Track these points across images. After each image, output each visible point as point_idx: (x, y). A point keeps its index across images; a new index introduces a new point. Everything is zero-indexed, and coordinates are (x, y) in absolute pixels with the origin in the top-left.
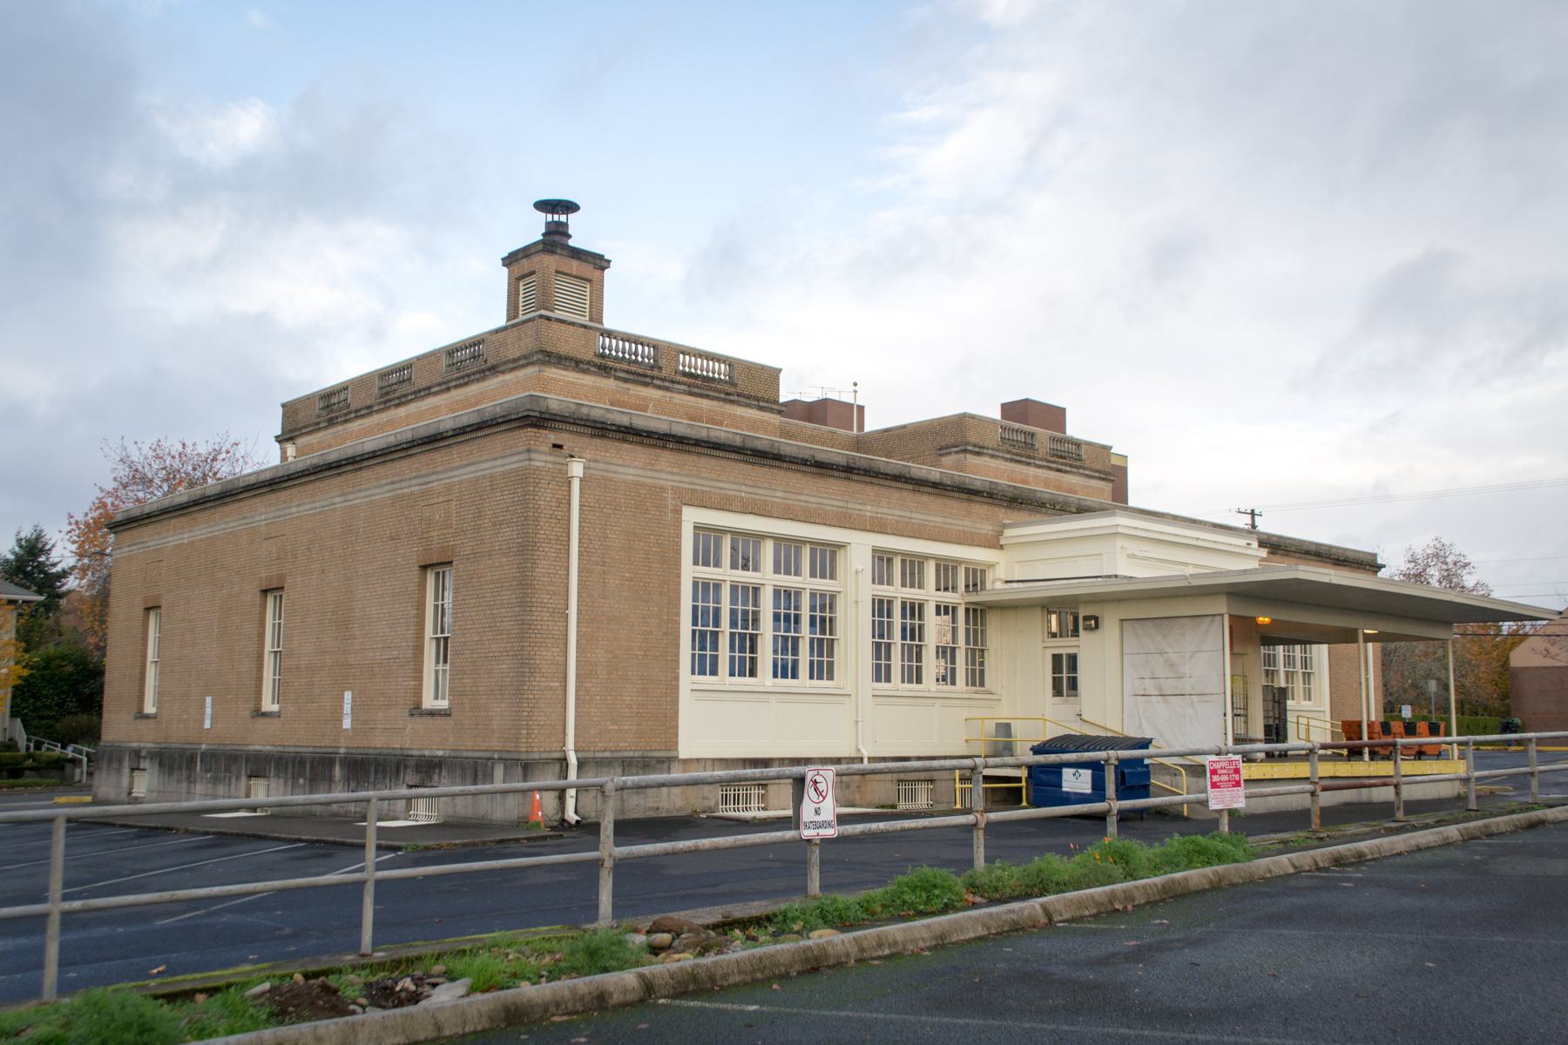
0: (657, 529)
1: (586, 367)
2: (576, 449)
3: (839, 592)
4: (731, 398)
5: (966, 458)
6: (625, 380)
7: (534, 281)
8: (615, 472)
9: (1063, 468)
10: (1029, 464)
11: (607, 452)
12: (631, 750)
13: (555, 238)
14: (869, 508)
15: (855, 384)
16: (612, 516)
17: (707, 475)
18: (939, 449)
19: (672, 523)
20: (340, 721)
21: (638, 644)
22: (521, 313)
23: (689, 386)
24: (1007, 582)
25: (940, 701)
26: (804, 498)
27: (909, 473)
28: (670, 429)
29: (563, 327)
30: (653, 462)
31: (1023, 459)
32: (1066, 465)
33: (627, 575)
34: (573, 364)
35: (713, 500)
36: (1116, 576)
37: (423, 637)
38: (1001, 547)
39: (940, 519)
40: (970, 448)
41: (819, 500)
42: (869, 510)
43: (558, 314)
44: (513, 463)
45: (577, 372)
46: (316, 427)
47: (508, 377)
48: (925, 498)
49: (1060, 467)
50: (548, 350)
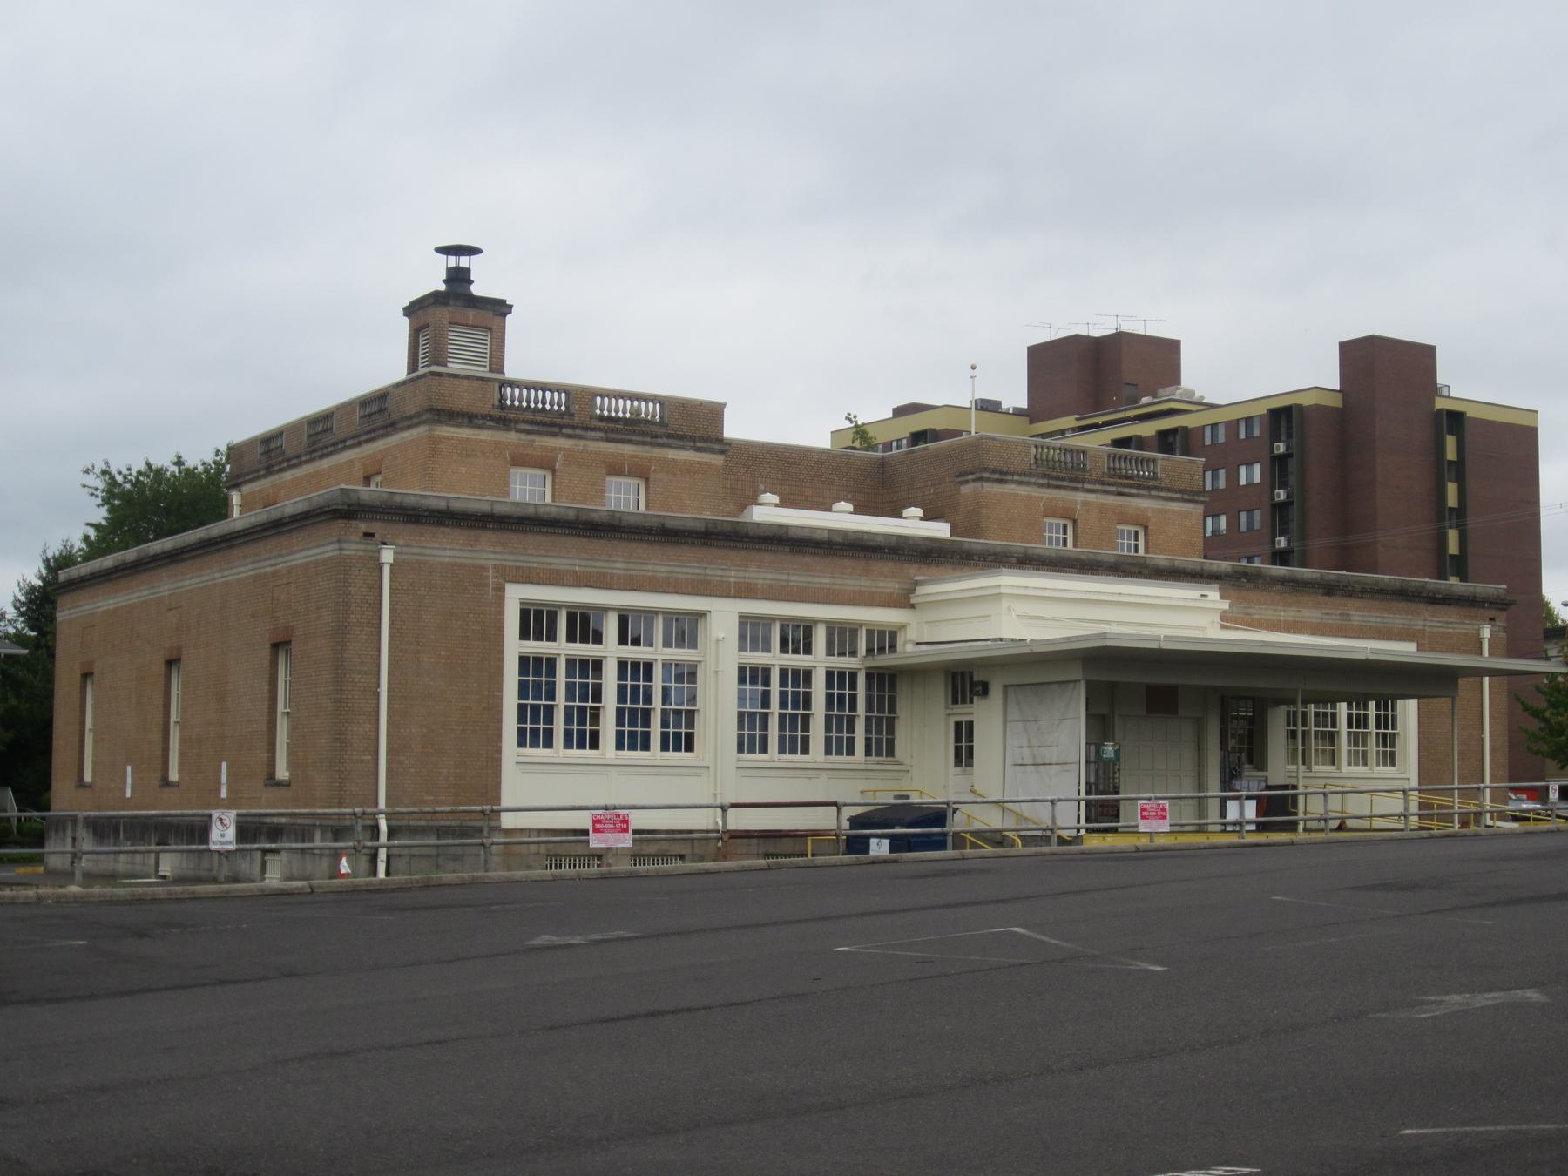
0: (476, 608)
1: (481, 422)
2: (389, 536)
3: (700, 662)
4: (660, 440)
5: (982, 487)
6: (528, 432)
7: (428, 334)
8: (430, 555)
9: (1126, 490)
10: (1075, 489)
11: (422, 535)
12: (448, 820)
13: (459, 278)
14: (733, 573)
15: (973, 368)
16: (427, 597)
17: (534, 551)
18: (958, 477)
19: (494, 601)
20: (219, 791)
21: (456, 719)
22: (420, 365)
23: (606, 432)
24: (918, 644)
25: (828, 772)
26: (650, 567)
27: (787, 534)
28: (492, 510)
29: (457, 382)
30: (472, 543)
31: (1066, 484)
32: (1130, 486)
33: (442, 653)
34: (466, 420)
35: (541, 575)
36: (1001, 639)
37: (276, 712)
38: (912, 606)
39: (827, 581)
40: (986, 475)
41: (669, 569)
42: (733, 576)
43: (453, 367)
44: (328, 551)
45: (472, 427)
46: (256, 475)
47: (406, 434)
48: (808, 559)
49: (1120, 489)
50: (439, 407)
